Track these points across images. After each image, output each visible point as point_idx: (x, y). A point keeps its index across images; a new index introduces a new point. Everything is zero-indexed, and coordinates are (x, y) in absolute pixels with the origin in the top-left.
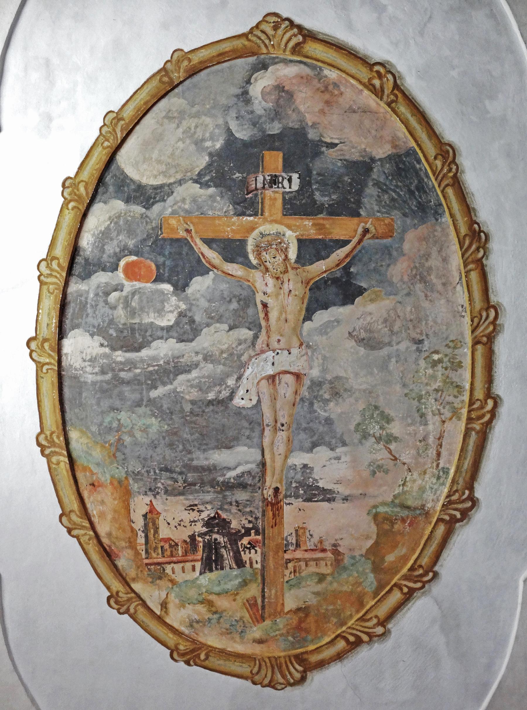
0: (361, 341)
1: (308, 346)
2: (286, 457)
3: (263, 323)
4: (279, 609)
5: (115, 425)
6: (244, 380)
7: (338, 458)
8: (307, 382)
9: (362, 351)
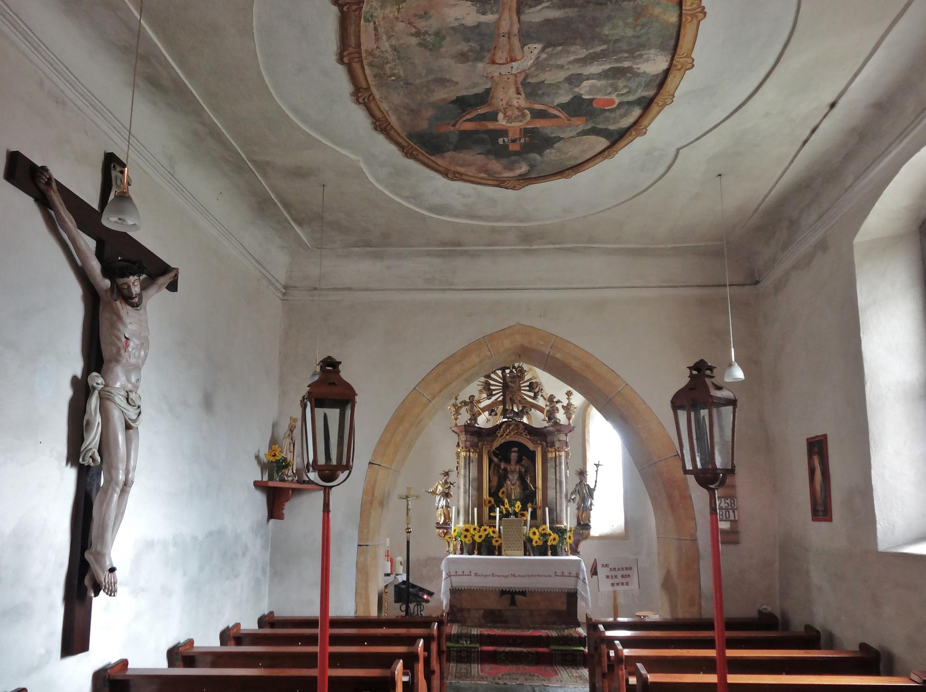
0: (448, 81)
1: (487, 77)
2: (500, 19)
3: (520, 86)
4: (568, 521)
5: (638, 28)
6: (534, 58)
7: (456, 19)
8: (486, 60)
9: (447, 77)
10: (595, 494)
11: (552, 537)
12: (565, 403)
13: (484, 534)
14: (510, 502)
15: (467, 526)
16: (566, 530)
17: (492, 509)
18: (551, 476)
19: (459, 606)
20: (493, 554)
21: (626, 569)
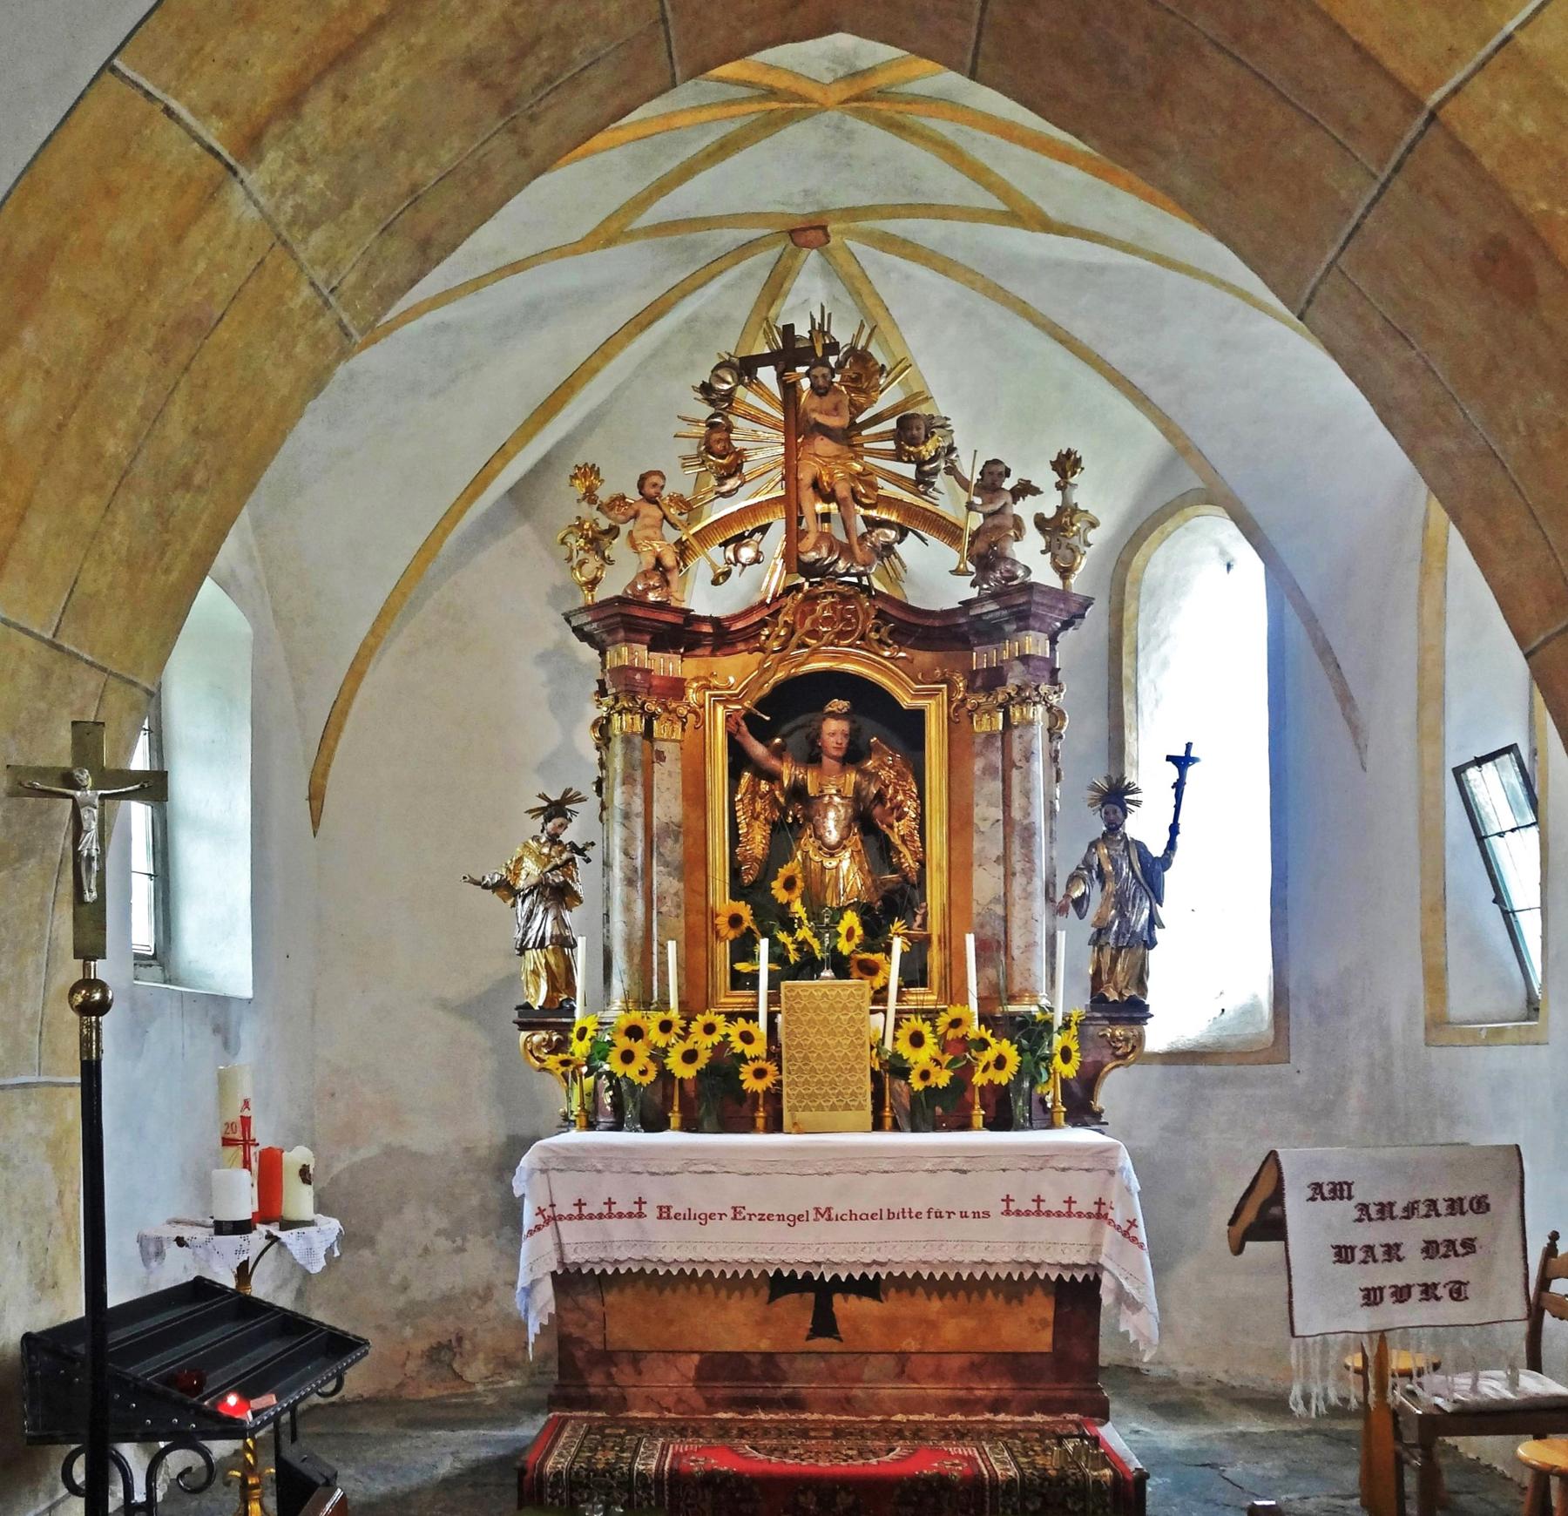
10: (1171, 879)
11: (990, 1055)
12: (1048, 504)
13: (704, 1044)
14: (814, 916)
15: (636, 1016)
16: (1048, 1025)
17: (743, 949)
18: (986, 812)
19: (596, 1342)
20: (749, 1127)
21: (1455, 1206)
